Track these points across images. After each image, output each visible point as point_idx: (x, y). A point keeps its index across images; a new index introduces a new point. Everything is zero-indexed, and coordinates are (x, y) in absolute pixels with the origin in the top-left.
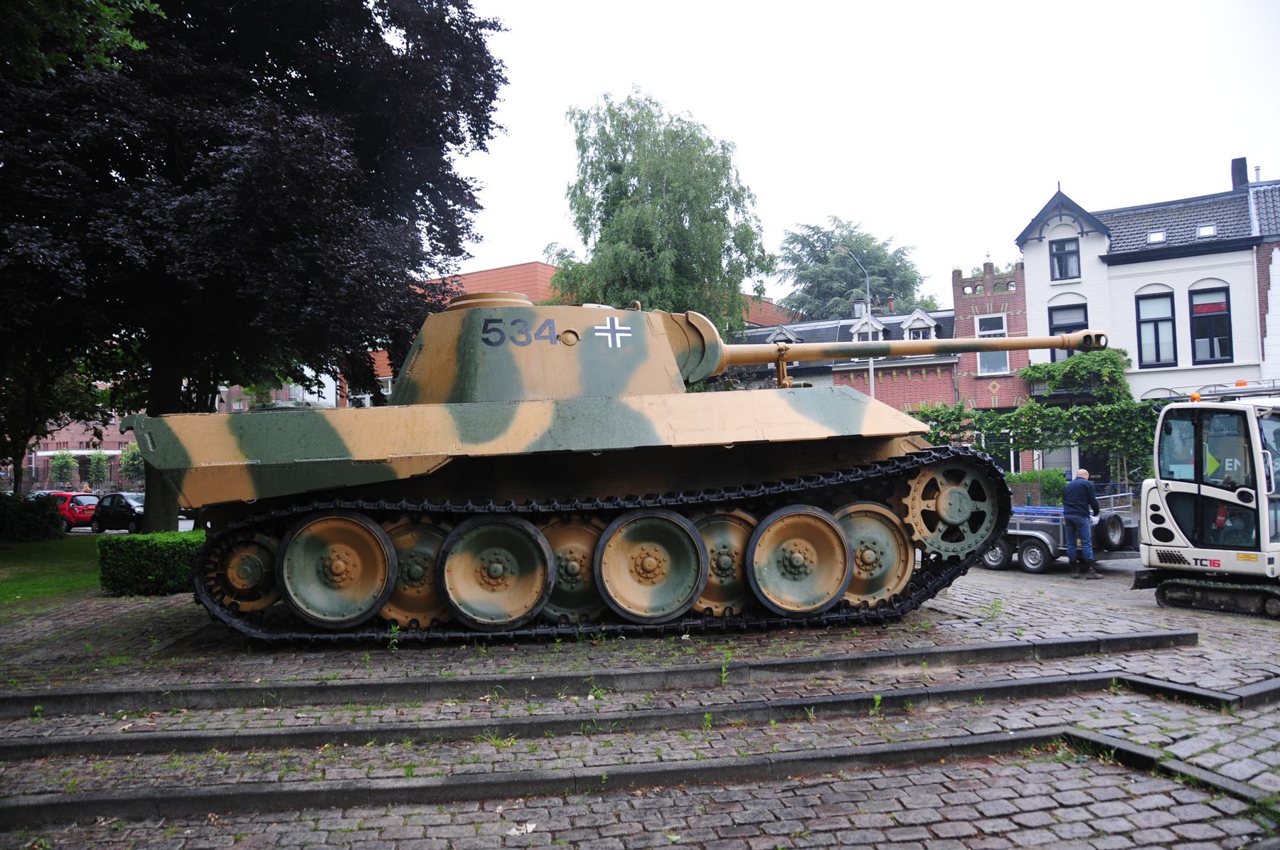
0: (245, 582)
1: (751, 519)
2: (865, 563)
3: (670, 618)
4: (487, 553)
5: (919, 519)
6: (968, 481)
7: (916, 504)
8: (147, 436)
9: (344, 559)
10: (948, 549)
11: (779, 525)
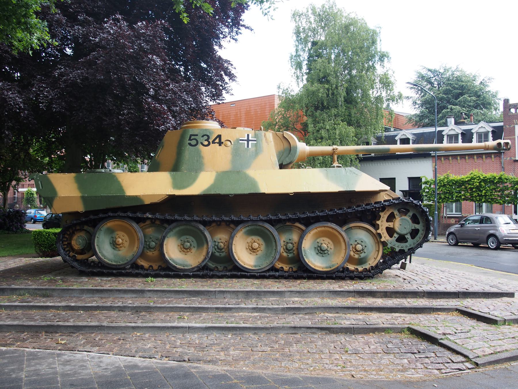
0: (78, 246)
1: (303, 227)
2: (357, 251)
3: (260, 271)
4: (184, 238)
5: (385, 231)
6: (410, 214)
7: (383, 224)
8: (39, 182)
9: (122, 238)
10: (398, 247)
11: (315, 231)
